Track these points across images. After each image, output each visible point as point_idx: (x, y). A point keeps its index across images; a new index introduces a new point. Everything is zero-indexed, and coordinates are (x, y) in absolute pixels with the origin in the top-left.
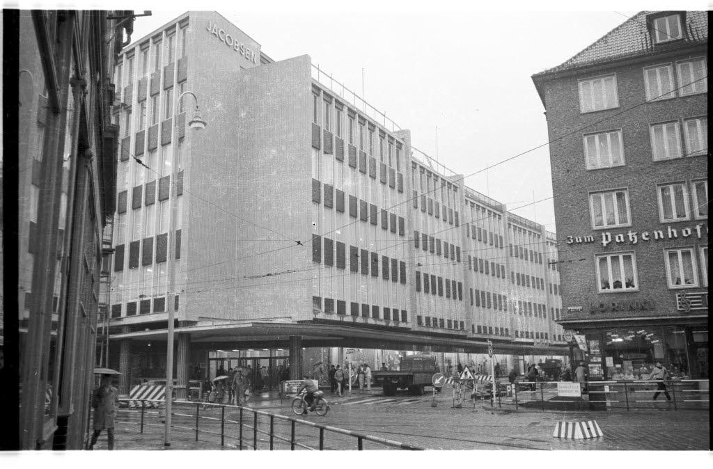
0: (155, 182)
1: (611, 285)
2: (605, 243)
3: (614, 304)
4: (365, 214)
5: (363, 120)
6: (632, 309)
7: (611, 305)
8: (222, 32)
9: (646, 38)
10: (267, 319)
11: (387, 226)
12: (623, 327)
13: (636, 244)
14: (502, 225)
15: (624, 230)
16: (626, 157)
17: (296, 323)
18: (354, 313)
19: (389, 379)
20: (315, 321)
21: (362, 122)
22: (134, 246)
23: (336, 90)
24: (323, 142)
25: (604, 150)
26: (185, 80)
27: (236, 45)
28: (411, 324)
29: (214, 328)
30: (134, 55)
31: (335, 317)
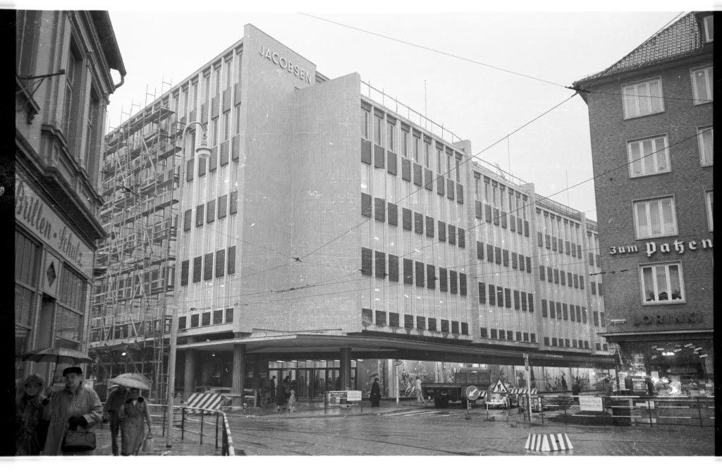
0: (214, 201)
1: (657, 297)
2: (649, 252)
3: (659, 317)
4: (417, 224)
5: (417, 133)
6: (678, 322)
7: (656, 317)
8: (276, 55)
9: (696, 37)
10: (317, 331)
11: (455, 241)
12: (667, 340)
13: (682, 254)
14: (581, 235)
15: (670, 239)
16: (672, 163)
17: (346, 335)
18: (409, 324)
19: (438, 391)
20: (365, 333)
21: (418, 135)
22: (197, 261)
23: (390, 106)
24: (372, 155)
25: (649, 155)
26: (240, 103)
27: (290, 66)
28: (473, 336)
29: (266, 339)
30: (197, 81)
31: (387, 329)
